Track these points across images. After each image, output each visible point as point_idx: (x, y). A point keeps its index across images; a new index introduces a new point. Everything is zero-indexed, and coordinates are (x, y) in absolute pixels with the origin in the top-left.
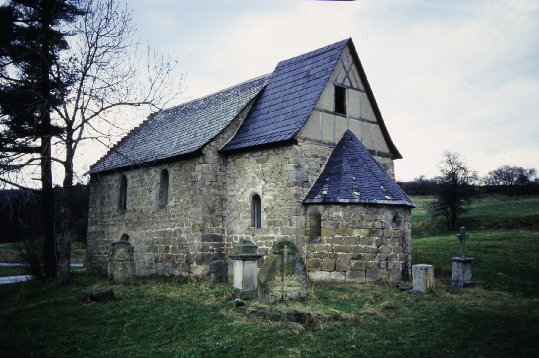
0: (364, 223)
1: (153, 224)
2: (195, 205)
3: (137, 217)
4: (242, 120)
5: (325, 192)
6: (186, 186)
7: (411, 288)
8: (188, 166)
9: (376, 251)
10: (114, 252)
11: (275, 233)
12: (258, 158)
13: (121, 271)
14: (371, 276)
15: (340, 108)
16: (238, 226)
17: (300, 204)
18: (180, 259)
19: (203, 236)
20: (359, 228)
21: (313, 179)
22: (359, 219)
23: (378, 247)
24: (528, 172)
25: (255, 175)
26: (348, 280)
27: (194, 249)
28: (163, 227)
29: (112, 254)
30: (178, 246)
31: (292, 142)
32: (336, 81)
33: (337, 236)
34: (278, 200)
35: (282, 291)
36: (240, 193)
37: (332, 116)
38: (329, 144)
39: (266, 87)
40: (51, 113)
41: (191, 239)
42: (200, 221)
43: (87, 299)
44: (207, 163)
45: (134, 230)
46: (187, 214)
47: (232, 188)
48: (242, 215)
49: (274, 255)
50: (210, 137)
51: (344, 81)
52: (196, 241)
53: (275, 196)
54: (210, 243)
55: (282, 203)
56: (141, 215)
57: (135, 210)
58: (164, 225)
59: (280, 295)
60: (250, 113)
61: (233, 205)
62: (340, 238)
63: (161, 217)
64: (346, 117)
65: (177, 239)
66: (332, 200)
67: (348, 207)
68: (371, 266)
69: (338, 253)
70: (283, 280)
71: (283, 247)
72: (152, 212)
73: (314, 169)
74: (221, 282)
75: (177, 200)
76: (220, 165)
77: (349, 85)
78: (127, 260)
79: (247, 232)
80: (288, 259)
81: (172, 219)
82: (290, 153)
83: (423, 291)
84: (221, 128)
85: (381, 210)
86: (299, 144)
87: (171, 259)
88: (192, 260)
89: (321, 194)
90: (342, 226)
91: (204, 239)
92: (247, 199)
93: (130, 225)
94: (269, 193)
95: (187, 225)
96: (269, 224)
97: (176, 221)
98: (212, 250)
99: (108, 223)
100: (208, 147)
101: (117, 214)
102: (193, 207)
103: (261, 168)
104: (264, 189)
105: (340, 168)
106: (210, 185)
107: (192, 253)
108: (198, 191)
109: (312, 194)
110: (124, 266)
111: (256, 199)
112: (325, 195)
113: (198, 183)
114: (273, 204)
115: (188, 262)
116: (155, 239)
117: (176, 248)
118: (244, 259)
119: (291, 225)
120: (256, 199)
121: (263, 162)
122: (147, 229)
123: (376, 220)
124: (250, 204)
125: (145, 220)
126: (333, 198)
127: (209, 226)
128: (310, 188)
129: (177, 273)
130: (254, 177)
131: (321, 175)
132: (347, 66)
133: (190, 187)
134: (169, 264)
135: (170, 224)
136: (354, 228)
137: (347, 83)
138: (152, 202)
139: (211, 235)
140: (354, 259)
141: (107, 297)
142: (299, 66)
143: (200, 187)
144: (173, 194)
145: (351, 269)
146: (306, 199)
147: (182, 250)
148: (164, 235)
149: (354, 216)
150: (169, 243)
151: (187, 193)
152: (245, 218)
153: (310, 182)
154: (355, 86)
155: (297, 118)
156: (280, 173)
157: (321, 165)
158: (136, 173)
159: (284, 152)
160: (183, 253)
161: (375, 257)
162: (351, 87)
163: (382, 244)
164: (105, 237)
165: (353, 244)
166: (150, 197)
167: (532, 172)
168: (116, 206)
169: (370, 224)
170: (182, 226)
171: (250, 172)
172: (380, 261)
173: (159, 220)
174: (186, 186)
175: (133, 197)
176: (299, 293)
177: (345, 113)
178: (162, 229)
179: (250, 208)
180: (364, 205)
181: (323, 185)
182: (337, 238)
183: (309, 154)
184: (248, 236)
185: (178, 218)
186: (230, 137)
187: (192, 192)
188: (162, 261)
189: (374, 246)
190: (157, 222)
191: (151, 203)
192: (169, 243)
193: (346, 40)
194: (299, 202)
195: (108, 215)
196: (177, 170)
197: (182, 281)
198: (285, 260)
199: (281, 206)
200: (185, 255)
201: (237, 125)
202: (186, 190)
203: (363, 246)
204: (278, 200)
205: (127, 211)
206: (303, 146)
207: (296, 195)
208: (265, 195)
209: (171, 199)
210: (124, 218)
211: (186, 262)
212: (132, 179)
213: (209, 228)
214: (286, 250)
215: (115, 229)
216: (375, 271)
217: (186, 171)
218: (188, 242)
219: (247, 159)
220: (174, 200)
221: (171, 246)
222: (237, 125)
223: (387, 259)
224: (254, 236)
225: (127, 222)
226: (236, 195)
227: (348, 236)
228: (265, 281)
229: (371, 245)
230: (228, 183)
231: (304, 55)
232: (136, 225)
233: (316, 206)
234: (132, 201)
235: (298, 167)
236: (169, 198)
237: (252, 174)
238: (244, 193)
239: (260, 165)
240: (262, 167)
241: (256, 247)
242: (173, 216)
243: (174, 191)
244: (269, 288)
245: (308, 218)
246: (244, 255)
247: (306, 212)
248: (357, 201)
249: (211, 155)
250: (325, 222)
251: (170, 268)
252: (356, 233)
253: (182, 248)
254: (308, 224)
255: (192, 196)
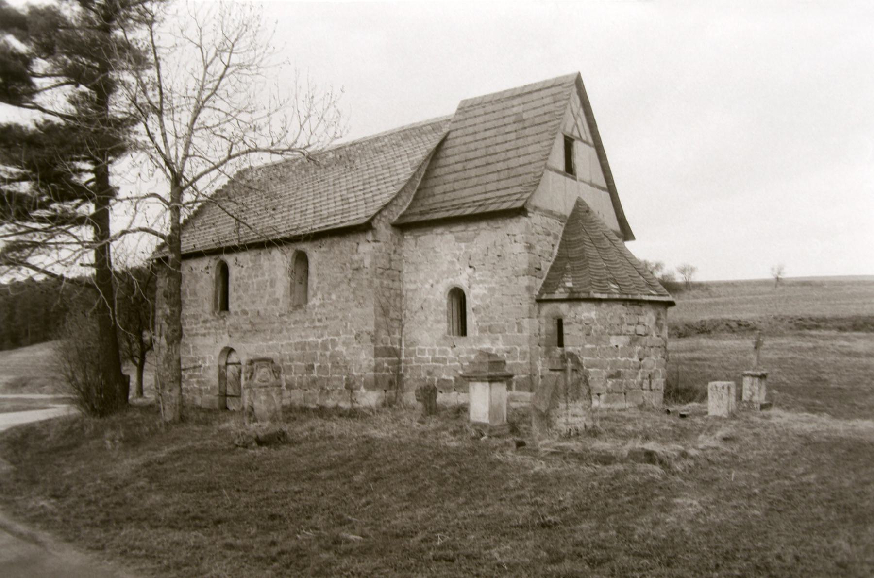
0: (624, 328)
1: (280, 332)
2: (360, 303)
3: (251, 322)
4: (419, 180)
5: (569, 284)
6: (342, 275)
7: (707, 413)
8: (346, 244)
9: (638, 366)
10: (252, 373)
11: (493, 343)
12: (460, 234)
13: (265, 401)
14: (632, 400)
15: (570, 169)
16: (426, 334)
17: (534, 301)
18: (336, 383)
19: (376, 349)
20: (617, 334)
21: (546, 266)
22: (618, 321)
23: (641, 360)
24: (654, 266)
25: (455, 260)
26: (603, 406)
27: (360, 368)
28: (301, 337)
29: (250, 377)
30: (330, 365)
31: (521, 212)
32: (564, 129)
33: (588, 346)
34: (497, 295)
35: (567, 424)
36: (428, 286)
37: (562, 177)
38: (561, 218)
39: (448, 133)
40: (109, 166)
41: (353, 354)
42: (371, 328)
43: (251, 443)
44: (378, 241)
45: (243, 342)
46: (345, 318)
47: (413, 279)
48: (431, 318)
49: (553, 373)
50: (379, 204)
51: (573, 130)
52: (363, 356)
53: (492, 290)
54: (384, 359)
55: (505, 299)
56: (258, 320)
57: (245, 313)
58: (303, 334)
59: (564, 429)
60: (428, 171)
61: (416, 305)
62: (593, 349)
63: (296, 322)
64: (576, 179)
65: (328, 353)
66: (583, 295)
67: (604, 305)
68: (632, 386)
69: (590, 370)
70: (567, 408)
71: (566, 361)
72: (277, 314)
73: (548, 250)
74: (431, 413)
75: (326, 296)
76: (394, 244)
77: (578, 136)
78: (273, 386)
79: (442, 342)
80: (571, 379)
81: (317, 324)
82: (516, 226)
83: (726, 416)
84: (394, 191)
85: (644, 309)
86: (530, 214)
87: (319, 383)
88: (358, 383)
89: (564, 287)
90: (596, 331)
91: (377, 353)
92: (440, 295)
93: (237, 335)
94: (481, 285)
95: (346, 333)
96: (482, 330)
97: (326, 327)
98: (388, 370)
99: (194, 332)
100: (378, 217)
101: (210, 318)
102: (357, 307)
103: (464, 250)
104: (471, 280)
105: (583, 250)
106: (382, 274)
107: (355, 374)
108: (365, 283)
109: (548, 286)
110: (268, 394)
111: (458, 296)
112: (570, 288)
113: (365, 270)
114: (488, 301)
115: (350, 387)
116: (285, 355)
117: (326, 367)
118: (492, 380)
119: (520, 331)
120: (458, 296)
121: (468, 240)
122: (271, 340)
123: (638, 324)
124: (445, 301)
125: (266, 327)
126: (584, 292)
127: (383, 335)
128: (544, 279)
129: (330, 403)
130: (452, 263)
131: (556, 260)
132: (575, 110)
133: (350, 276)
134: (316, 391)
135: (315, 331)
136: (610, 335)
137: (576, 133)
138: (278, 300)
139: (385, 348)
140: (611, 377)
141: (279, 439)
142: (499, 106)
143: (368, 277)
144: (318, 288)
145: (608, 392)
146: (541, 294)
147: (338, 370)
148: (303, 348)
149: (611, 317)
150: (314, 359)
151: (344, 286)
152: (439, 322)
153: (543, 269)
154: (584, 138)
155: (520, 178)
156: (499, 256)
157: (553, 245)
158: (245, 257)
159: (506, 225)
160: (339, 373)
161: (637, 374)
162: (580, 139)
163: (645, 355)
164: (189, 352)
165: (610, 356)
166: (274, 293)
167: (658, 266)
168: (208, 306)
169: (632, 329)
170: (338, 334)
171: (446, 255)
172: (643, 378)
173: (293, 326)
174: (342, 275)
175: (241, 293)
176: (585, 427)
177: (575, 175)
178: (298, 340)
179: (446, 308)
180: (624, 301)
181: (563, 274)
182: (589, 349)
183: (539, 229)
184: (444, 348)
185: (328, 323)
186: (405, 203)
187: (353, 285)
188: (300, 386)
189: (636, 359)
190: (288, 330)
191: (276, 301)
192: (314, 359)
193: (572, 75)
194: (532, 298)
195: (193, 320)
196: (324, 252)
197: (353, 414)
198: (569, 379)
199: (502, 304)
200: (344, 377)
201: (413, 187)
202: (342, 282)
203: (623, 359)
204: (496, 296)
205: (229, 313)
206: (535, 218)
207: (529, 289)
208: (474, 289)
209: (315, 295)
210: (224, 323)
211: (346, 387)
212: (240, 266)
213: (383, 336)
214: (570, 365)
215: (210, 341)
216: (636, 393)
217: (341, 253)
218: (348, 358)
219: (439, 237)
220: (319, 295)
221: (316, 365)
222: (413, 187)
223: (650, 376)
224: (455, 349)
225: (231, 330)
226: (421, 289)
227: (604, 346)
228: (548, 410)
229: (632, 357)
230: (405, 271)
231: (505, 91)
232: (248, 334)
233: (555, 304)
234: (239, 298)
235: (530, 247)
236: (311, 293)
237: (449, 258)
238: (435, 286)
239: (463, 245)
240: (467, 247)
241: (505, 363)
242: (320, 320)
243: (319, 283)
244: (553, 419)
245: (544, 320)
246: (493, 373)
247: (539, 313)
248: (617, 296)
249: (383, 229)
250: (570, 326)
251: (317, 396)
252: (614, 341)
253: (337, 367)
254: (543, 330)
255: (355, 289)
